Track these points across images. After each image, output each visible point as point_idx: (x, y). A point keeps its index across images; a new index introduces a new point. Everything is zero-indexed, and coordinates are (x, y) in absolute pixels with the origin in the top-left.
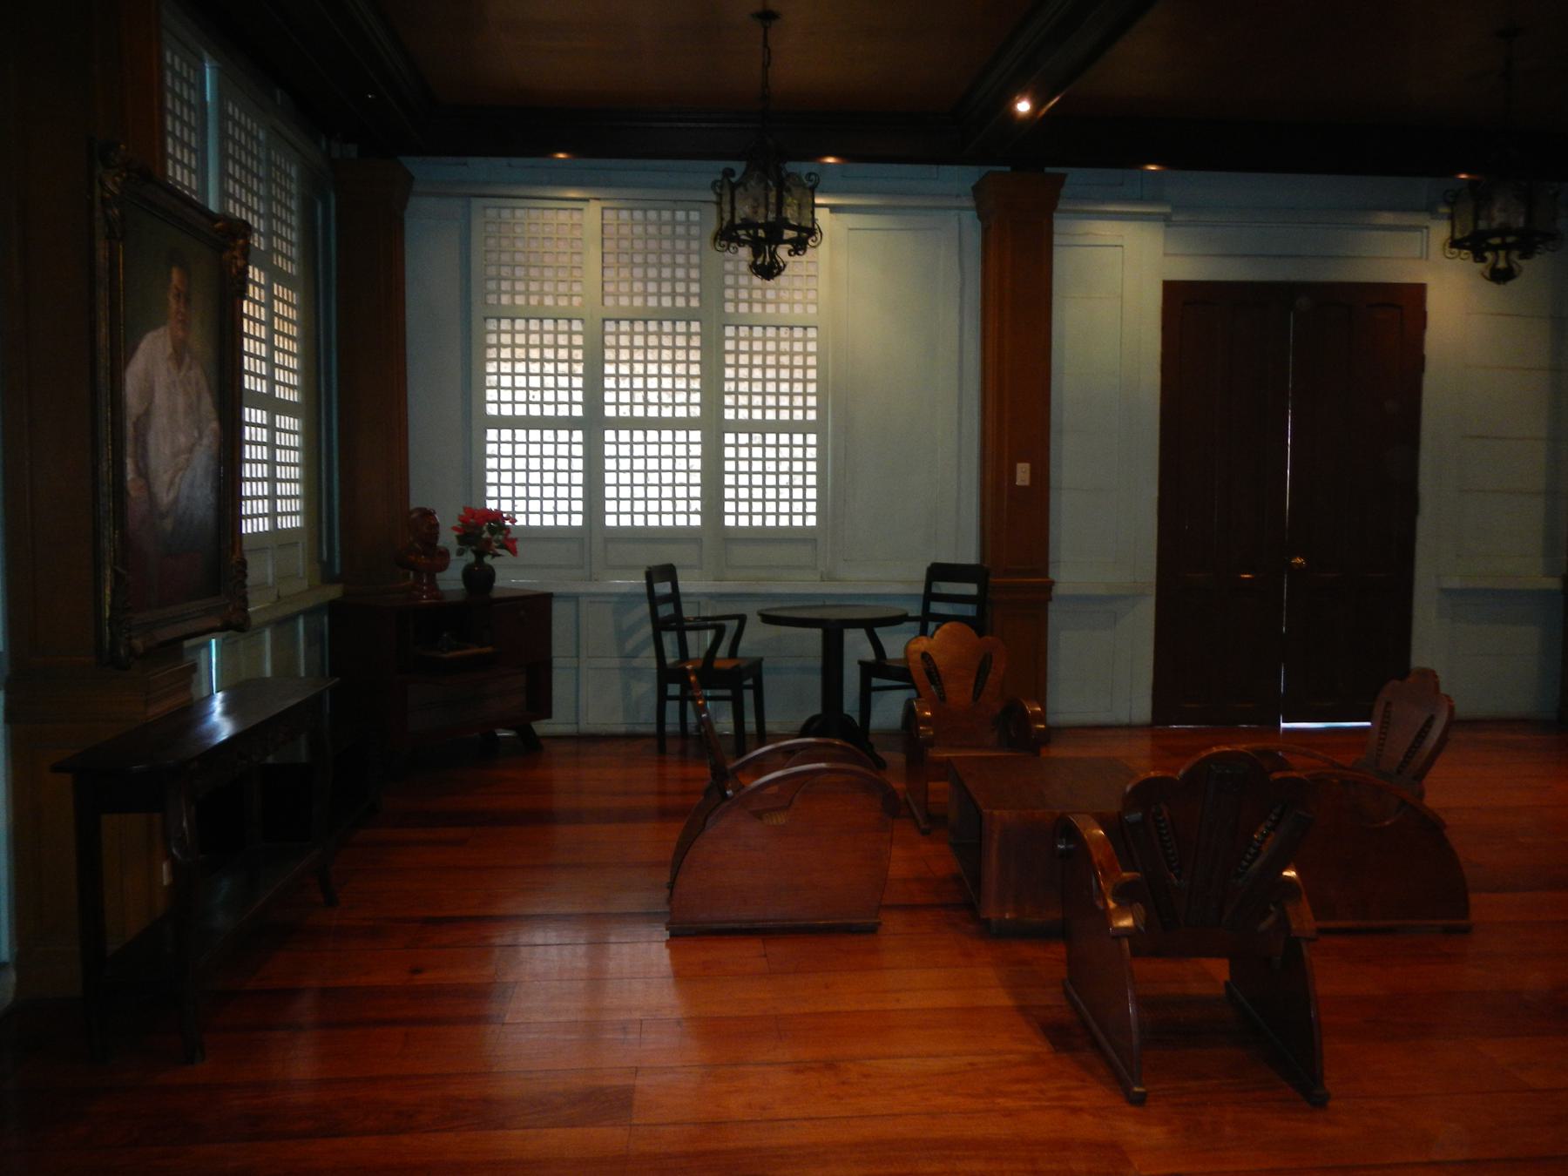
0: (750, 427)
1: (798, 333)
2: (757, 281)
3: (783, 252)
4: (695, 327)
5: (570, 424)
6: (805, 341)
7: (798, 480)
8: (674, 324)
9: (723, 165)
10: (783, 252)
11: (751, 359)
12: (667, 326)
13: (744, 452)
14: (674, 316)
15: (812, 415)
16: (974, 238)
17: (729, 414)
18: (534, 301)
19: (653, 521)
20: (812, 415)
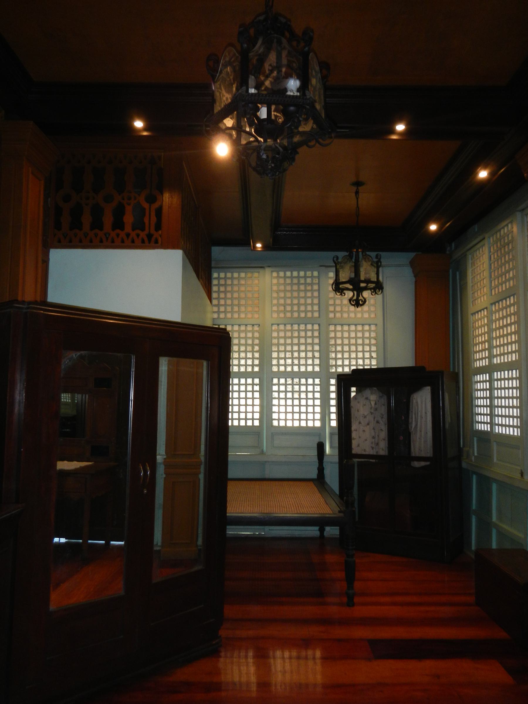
0: (285, 375)
1: (249, 328)
2: (352, 308)
3: (349, 294)
4: (316, 327)
5: (313, 375)
6: (253, 332)
7: (310, 409)
8: (306, 325)
9: (376, 253)
10: (349, 294)
11: (350, 348)
12: (296, 327)
13: (282, 388)
14: (306, 321)
15: (256, 369)
16: (411, 288)
17: (275, 369)
18: (345, 315)
19: (289, 424)
20: (256, 369)
